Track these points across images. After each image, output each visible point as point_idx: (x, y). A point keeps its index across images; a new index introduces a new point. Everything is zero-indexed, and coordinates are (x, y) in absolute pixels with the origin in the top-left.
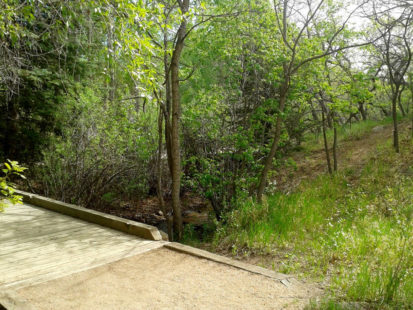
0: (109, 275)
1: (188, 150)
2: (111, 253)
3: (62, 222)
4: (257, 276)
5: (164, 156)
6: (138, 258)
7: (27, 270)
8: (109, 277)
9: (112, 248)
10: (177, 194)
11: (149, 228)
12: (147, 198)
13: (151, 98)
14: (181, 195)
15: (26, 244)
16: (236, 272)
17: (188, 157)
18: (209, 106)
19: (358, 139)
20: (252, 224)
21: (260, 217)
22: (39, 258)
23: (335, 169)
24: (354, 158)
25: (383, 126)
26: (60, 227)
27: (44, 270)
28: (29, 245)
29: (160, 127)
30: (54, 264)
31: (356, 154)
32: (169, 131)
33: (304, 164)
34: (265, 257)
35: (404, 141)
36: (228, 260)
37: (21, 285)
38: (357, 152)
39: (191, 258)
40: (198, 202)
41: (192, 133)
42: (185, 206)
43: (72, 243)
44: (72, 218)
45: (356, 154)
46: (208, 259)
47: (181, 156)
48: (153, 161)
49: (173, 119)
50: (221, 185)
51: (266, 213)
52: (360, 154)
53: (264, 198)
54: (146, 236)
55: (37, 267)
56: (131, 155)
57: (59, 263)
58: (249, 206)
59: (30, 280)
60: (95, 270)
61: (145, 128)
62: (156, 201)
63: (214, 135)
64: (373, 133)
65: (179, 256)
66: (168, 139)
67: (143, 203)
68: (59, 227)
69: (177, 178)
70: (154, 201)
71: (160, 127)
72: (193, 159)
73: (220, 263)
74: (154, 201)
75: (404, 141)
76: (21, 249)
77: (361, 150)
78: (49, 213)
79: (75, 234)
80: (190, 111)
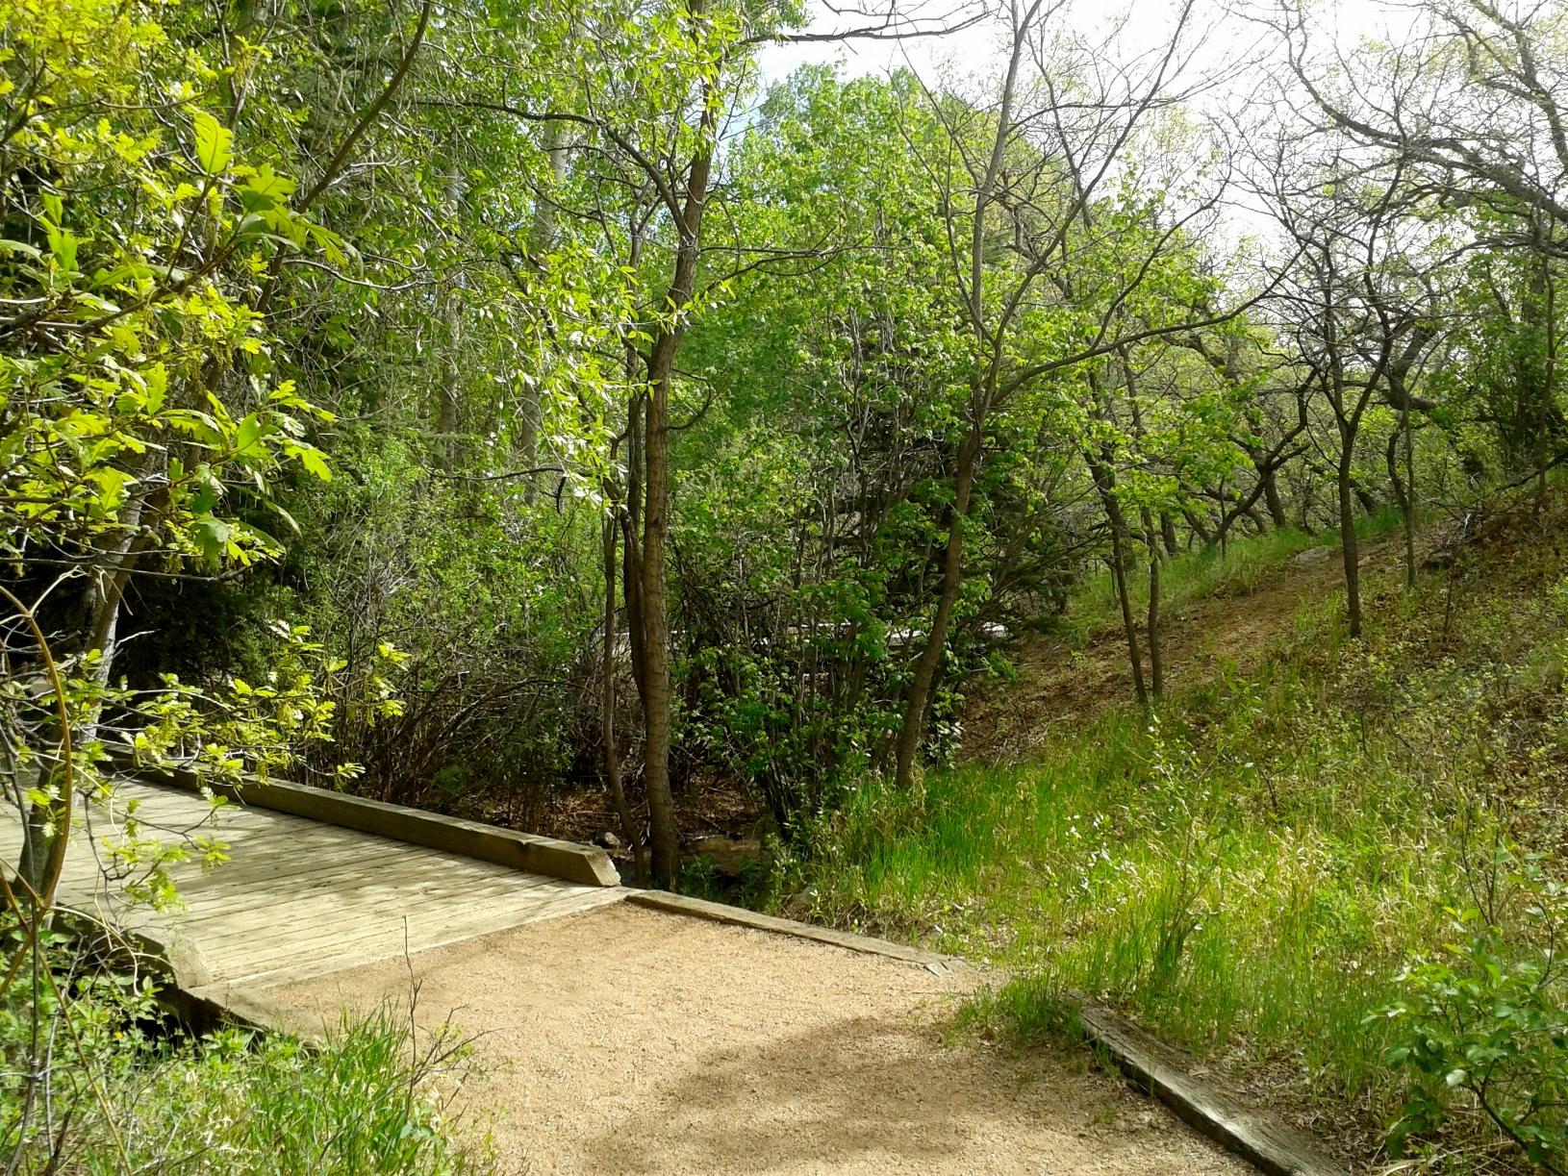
0: (487, 959)
1: (694, 630)
2: (487, 914)
3: (332, 846)
4: (868, 957)
5: (622, 650)
6: (558, 926)
7: (273, 952)
8: (489, 963)
9: (488, 902)
10: (662, 781)
11: (586, 853)
12: (566, 791)
13: (598, 498)
14: (677, 782)
15: (247, 897)
16: (818, 949)
17: (693, 650)
18: (763, 478)
19: (1243, 593)
20: (877, 845)
21: (902, 827)
22: (296, 925)
23: (1157, 688)
24: (1225, 652)
25: (1328, 548)
26: (334, 856)
27: (333, 928)
28: (259, 898)
29: (610, 560)
30: (338, 938)
31: (1230, 643)
32: (636, 571)
33: (1071, 675)
34: (903, 927)
35: (1381, 598)
36: (802, 928)
37: (269, 979)
38: (1234, 635)
39: (700, 924)
40: (732, 804)
41: (705, 576)
42: (690, 818)
43: (375, 894)
44: (358, 836)
45: (1230, 643)
46: (747, 925)
47: (673, 652)
48: (584, 670)
49: (646, 536)
50: (795, 738)
51: (921, 816)
52: (1240, 642)
53: (917, 773)
54: (575, 873)
55: (297, 945)
56: (516, 647)
57: (352, 937)
58: (870, 796)
59: (289, 970)
60: (452, 949)
61: (558, 558)
62: (595, 802)
63: (774, 581)
64: (1295, 571)
65: (666, 920)
66: (632, 596)
67: (553, 809)
68: (328, 857)
69: (661, 713)
70: (588, 801)
71: (610, 560)
72: (709, 652)
73: (778, 932)
74: (588, 801)
75: (1381, 598)
76: (238, 907)
77: (1249, 629)
78: (285, 824)
79: (378, 872)
80: (698, 499)
